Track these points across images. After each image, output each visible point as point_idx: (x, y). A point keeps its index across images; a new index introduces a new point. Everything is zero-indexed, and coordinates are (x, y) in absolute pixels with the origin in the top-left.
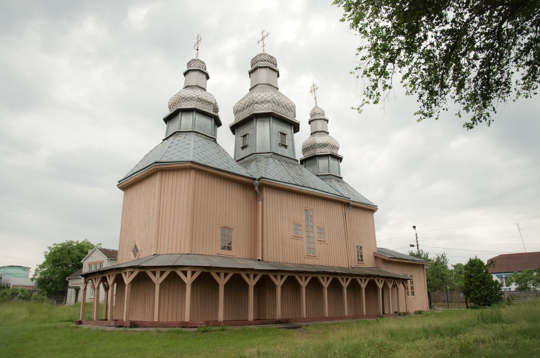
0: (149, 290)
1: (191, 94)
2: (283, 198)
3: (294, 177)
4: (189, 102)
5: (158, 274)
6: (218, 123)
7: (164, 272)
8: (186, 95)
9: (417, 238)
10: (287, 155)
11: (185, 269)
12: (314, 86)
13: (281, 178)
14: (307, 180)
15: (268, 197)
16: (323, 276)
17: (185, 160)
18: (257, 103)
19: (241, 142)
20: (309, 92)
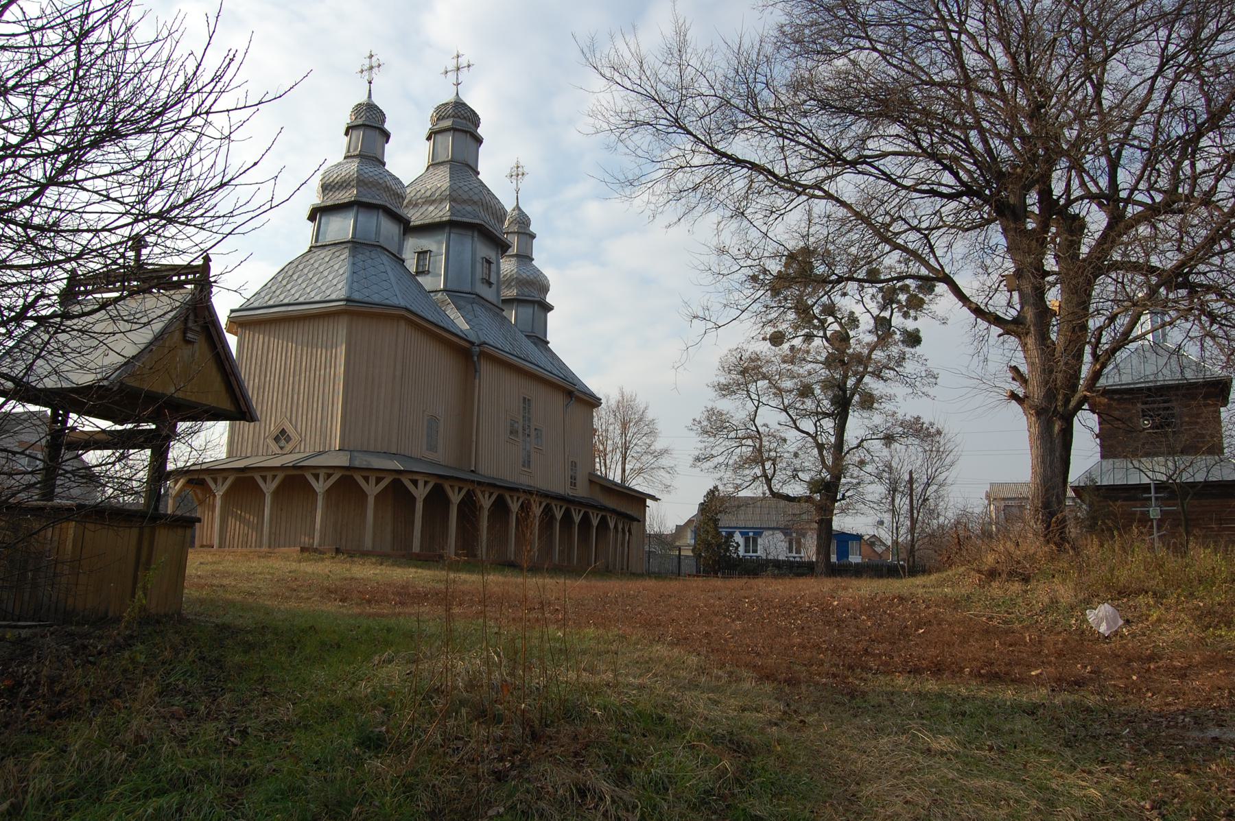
11: (415, 477)
12: (518, 167)
15: (487, 371)
16: (263, 474)
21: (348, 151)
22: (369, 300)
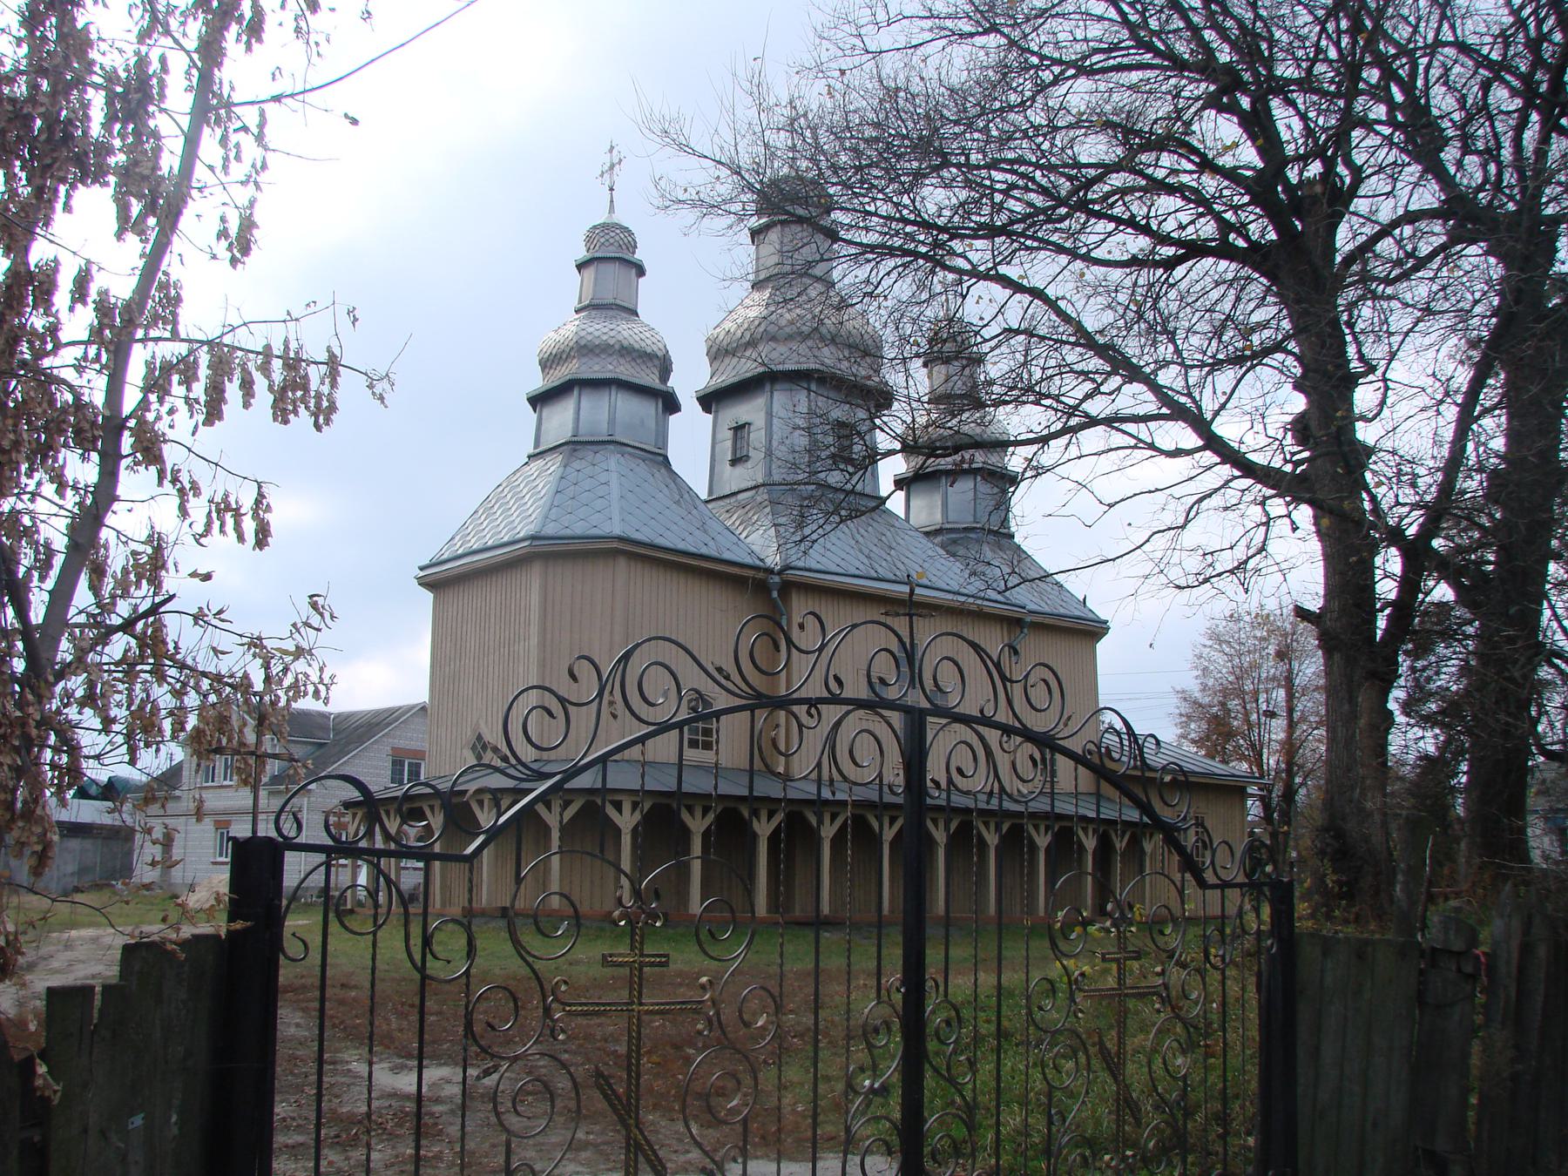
2: (842, 612)
3: (872, 555)
4: (596, 360)
6: (671, 404)
11: (617, 797)
13: (838, 561)
14: (906, 561)
16: (431, 803)
21: (580, 302)
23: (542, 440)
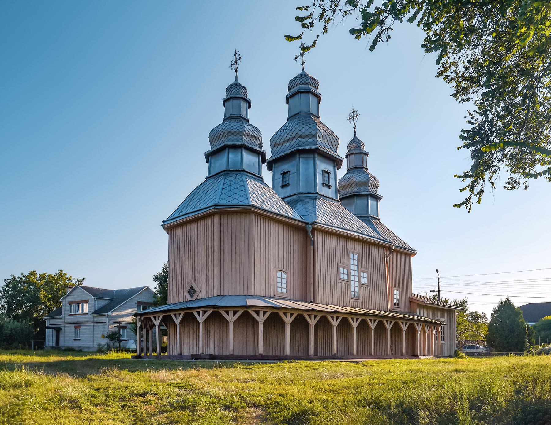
0: (214, 328)
1: (238, 128)
5: (231, 313)
7: (237, 312)
8: (232, 128)
9: (439, 283)
10: (330, 196)
11: (257, 309)
12: (353, 112)
17: (244, 204)
18: (300, 137)
19: (281, 180)
20: (347, 120)
22: (230, 204)
23: (211, 172)
